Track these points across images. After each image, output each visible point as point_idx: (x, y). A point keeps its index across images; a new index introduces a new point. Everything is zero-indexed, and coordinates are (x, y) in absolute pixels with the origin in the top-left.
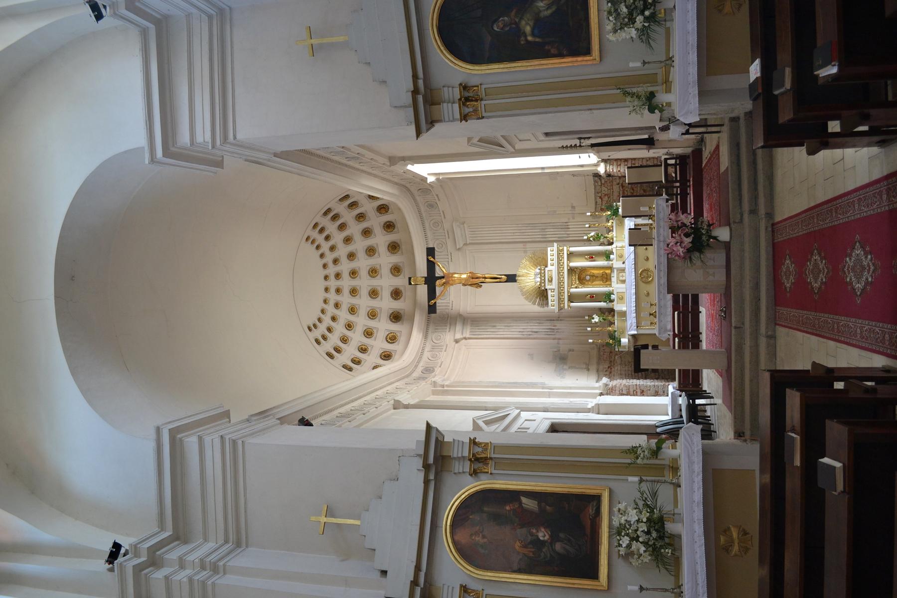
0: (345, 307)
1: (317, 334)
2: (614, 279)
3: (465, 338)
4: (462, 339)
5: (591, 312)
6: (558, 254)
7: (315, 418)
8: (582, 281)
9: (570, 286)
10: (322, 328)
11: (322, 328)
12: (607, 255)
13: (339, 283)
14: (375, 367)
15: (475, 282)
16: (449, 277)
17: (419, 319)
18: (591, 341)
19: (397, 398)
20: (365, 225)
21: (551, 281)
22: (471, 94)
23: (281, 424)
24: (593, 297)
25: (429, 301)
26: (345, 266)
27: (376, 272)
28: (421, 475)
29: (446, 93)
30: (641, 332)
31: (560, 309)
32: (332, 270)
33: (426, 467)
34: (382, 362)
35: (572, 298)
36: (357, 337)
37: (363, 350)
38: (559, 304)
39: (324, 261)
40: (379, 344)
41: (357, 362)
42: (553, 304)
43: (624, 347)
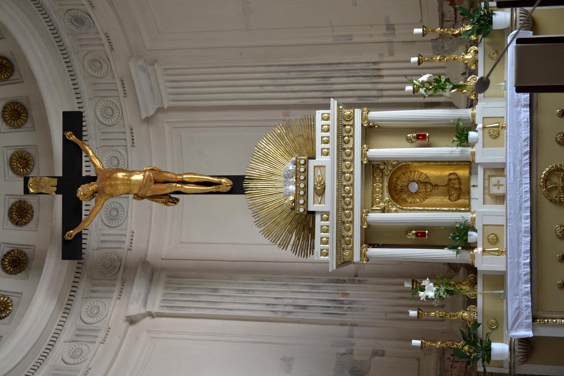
2: (477, 193)
3: (151, 315)
4: (144, 316)
5: (418, 273)
6: (341, 127)
8: (398, 195)
9: (367, 207)
12: (461, 132)
15: (164, 191)
17: (53, 265)
18: (416, 342)
21: (321, 192)
24: (423, 236)
25: (64, 233)
30: (545, 332)
31: (343, 262)
35: (372, 236)
38: (340, 249)
42: (324, 250)
43: (500, 364)
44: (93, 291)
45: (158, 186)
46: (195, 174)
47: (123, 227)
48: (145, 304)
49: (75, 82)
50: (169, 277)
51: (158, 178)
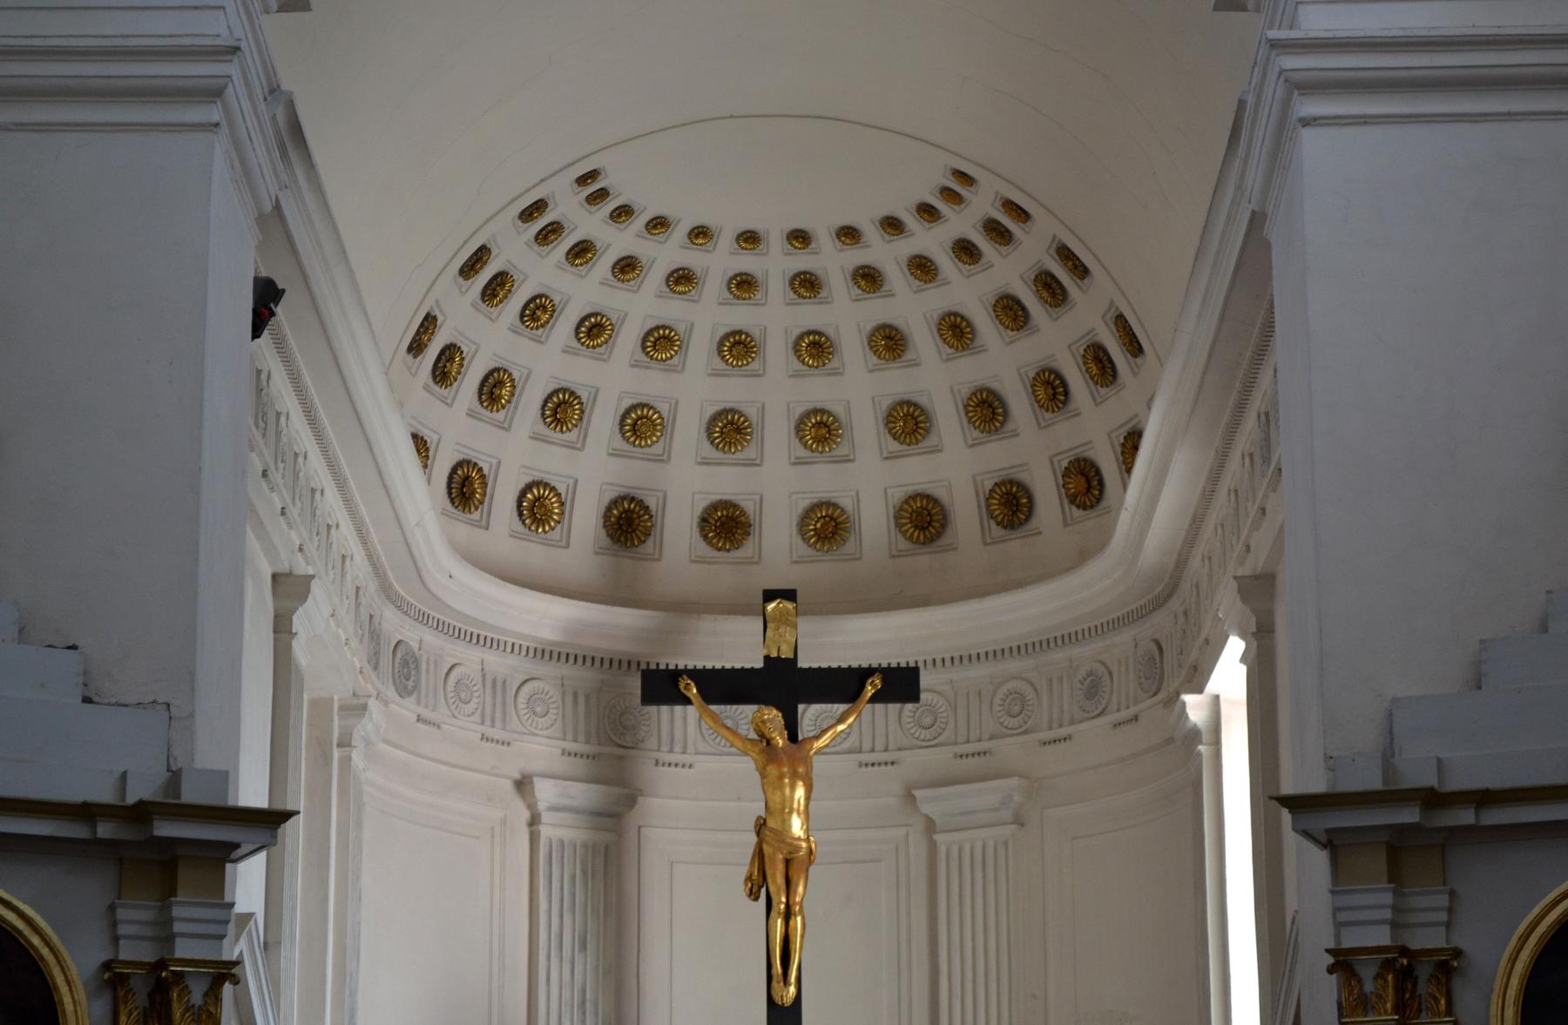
0: (673, 310)
1: (568, 206)
3: (534, 821)
4: (532, 807)
7: (280, 344)
10: (587, 223)
11: (587, 223)
13: (776, 352)
14: (421, 445)
15: (772, 871)
16: (794, 761)
19: (315, 586)
20: (1020, 405)
22: (1423, 988)
23: (261, 220)
26: (846, 316)
27: (820, 440)
28: (103, 794)
29: (1429, 902)
32: (832, 262)
33: (142, 813)
34: (442, 467)
36: (546, 362)
37: (494, 389)
39: (871, 233)
40: (515, 451)
41: (444, 372)
44: (575, 695)
45: (781, 867)
46: (802, 936)
47: (702, 747)
48: (554, 809)
49: (983, 657)
50: (607, 848)
51: (795, 864)
